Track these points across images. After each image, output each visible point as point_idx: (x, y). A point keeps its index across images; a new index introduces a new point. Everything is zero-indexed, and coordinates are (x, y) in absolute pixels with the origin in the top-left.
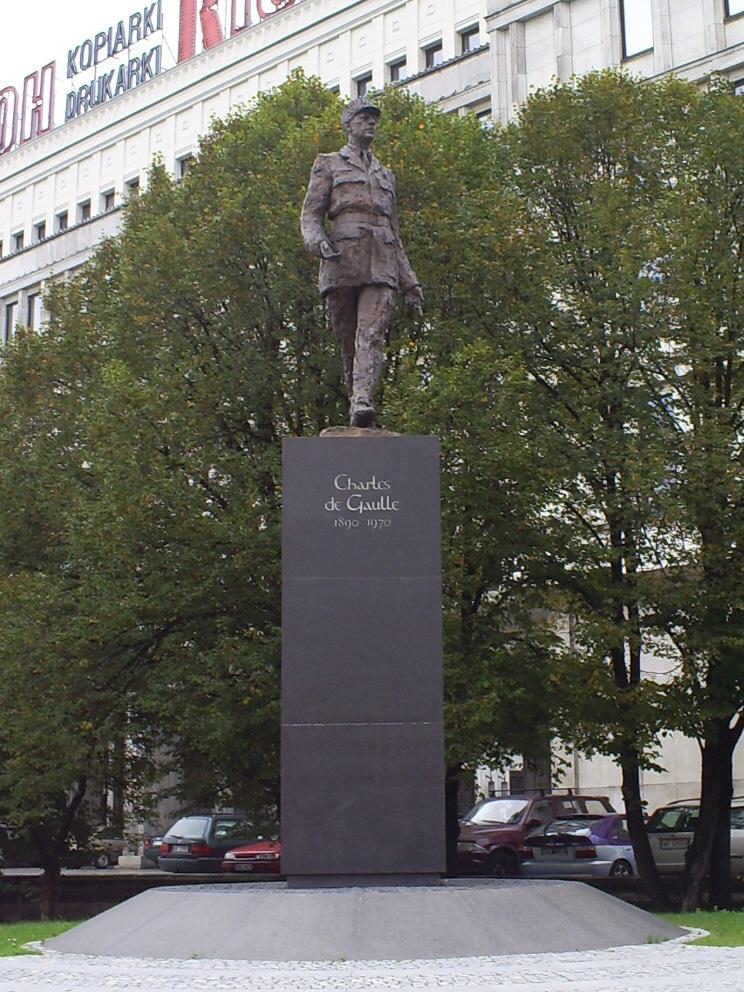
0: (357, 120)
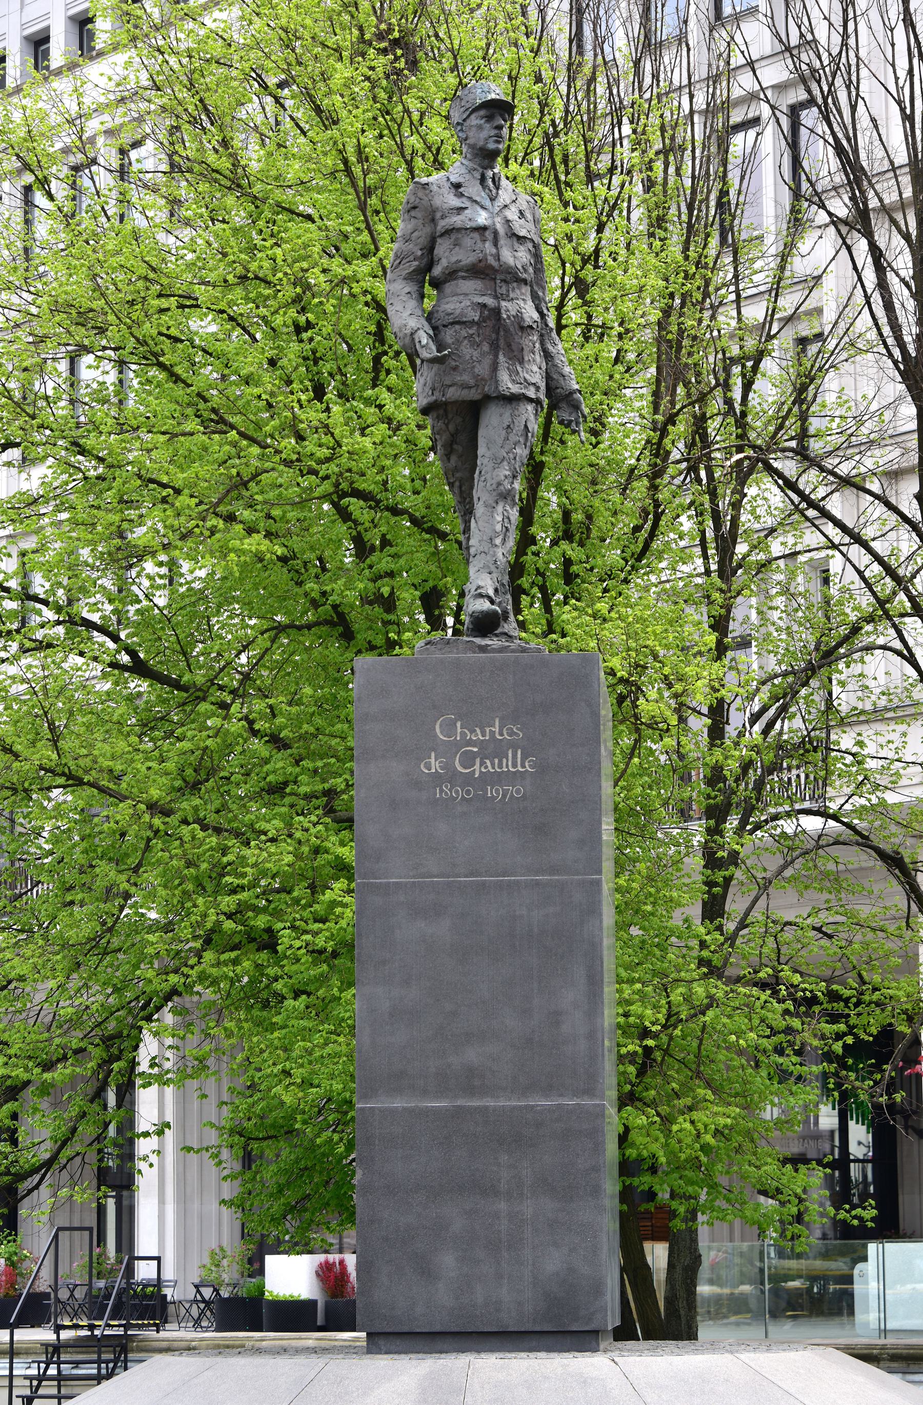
0: (474, 120)
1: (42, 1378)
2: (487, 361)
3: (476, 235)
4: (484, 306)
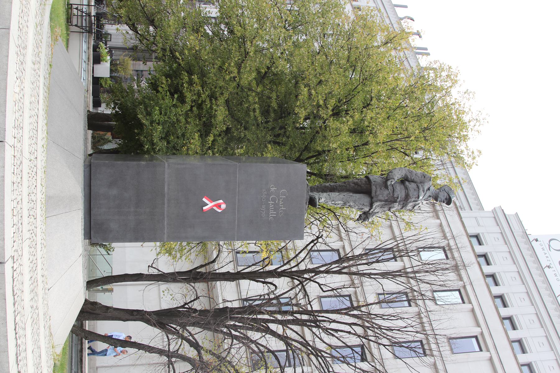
0: (446, 194)
1: (82, 12)
2: (383, 199)
3: (417, 196)
4: (398, 198)
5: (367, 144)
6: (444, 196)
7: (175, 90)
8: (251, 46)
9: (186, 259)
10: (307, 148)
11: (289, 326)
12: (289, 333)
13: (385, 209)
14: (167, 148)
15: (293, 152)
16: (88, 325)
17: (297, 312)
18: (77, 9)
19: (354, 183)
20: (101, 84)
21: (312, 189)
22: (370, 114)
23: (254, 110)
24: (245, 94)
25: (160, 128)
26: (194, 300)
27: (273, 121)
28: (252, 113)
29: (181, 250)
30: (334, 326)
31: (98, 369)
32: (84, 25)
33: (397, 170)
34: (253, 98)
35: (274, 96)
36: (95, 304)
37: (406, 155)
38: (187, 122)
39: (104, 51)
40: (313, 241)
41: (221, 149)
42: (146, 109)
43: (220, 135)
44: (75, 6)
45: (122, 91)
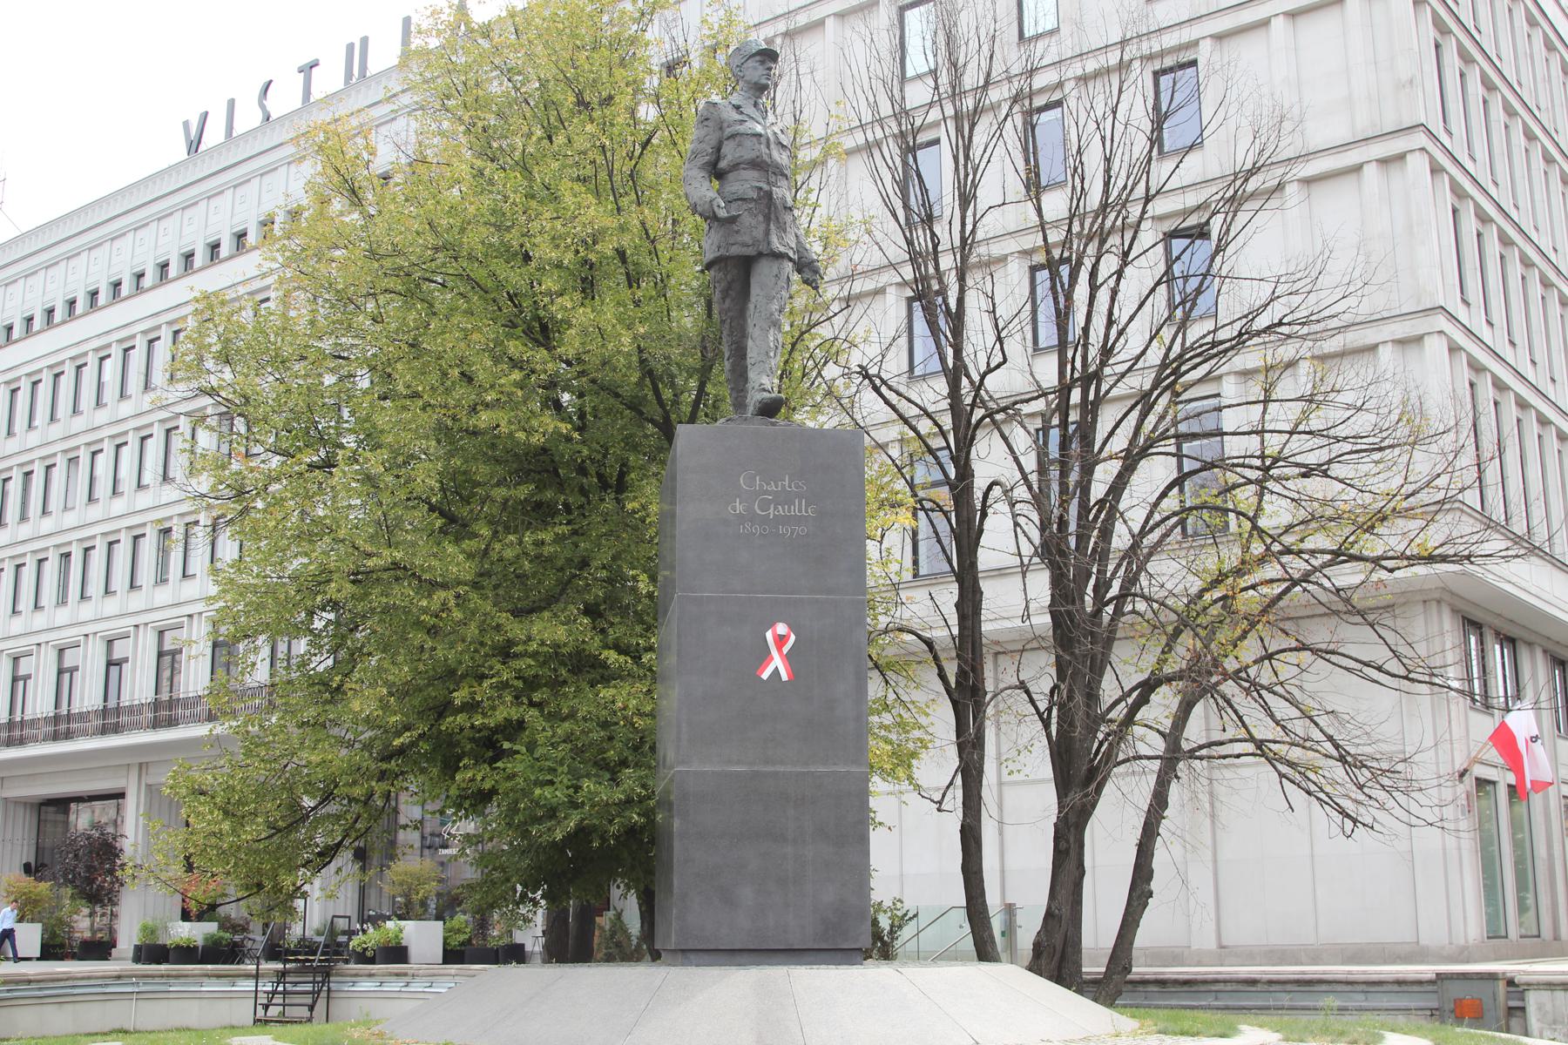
0: (750, 63)
1: (274, 992)
2: (762, 227)
5: (621, 254)
6: (755, 68)
7: (491, 746)
8: (378, 555)
9: (927, 715)
10: (635, 406)
11: (1096, 449)
12: (1119, 443)
13: (788, 218)
14: (637, 765)
15: (644, 441)
16: (1093, 965)
17: (1064, 424)
18: (266, 1007)
19: (724, 299)
20: (462, 944)
21: (740, 405)
22: (544, 251)
23: (540, 544)
24: (498, 568)
25: (586, 784)
26: (1028, 692)
27: (562, 491)
28: (547, 550)
29: (901, 725)
30: (1096, 337)
31: (1225, 943)
32: (309, 987)
33: (690, 190)
34: (507, 548)
35: (500, 493)
36: (1037, 947)
37: (649, 141)
38: (572, 715)
39: (372, 937)
40: (877, 390)
41: (638, 629)
42: (539, 820)
43: (603, 631)
44: (261, 1012)
45: (488, 883)
